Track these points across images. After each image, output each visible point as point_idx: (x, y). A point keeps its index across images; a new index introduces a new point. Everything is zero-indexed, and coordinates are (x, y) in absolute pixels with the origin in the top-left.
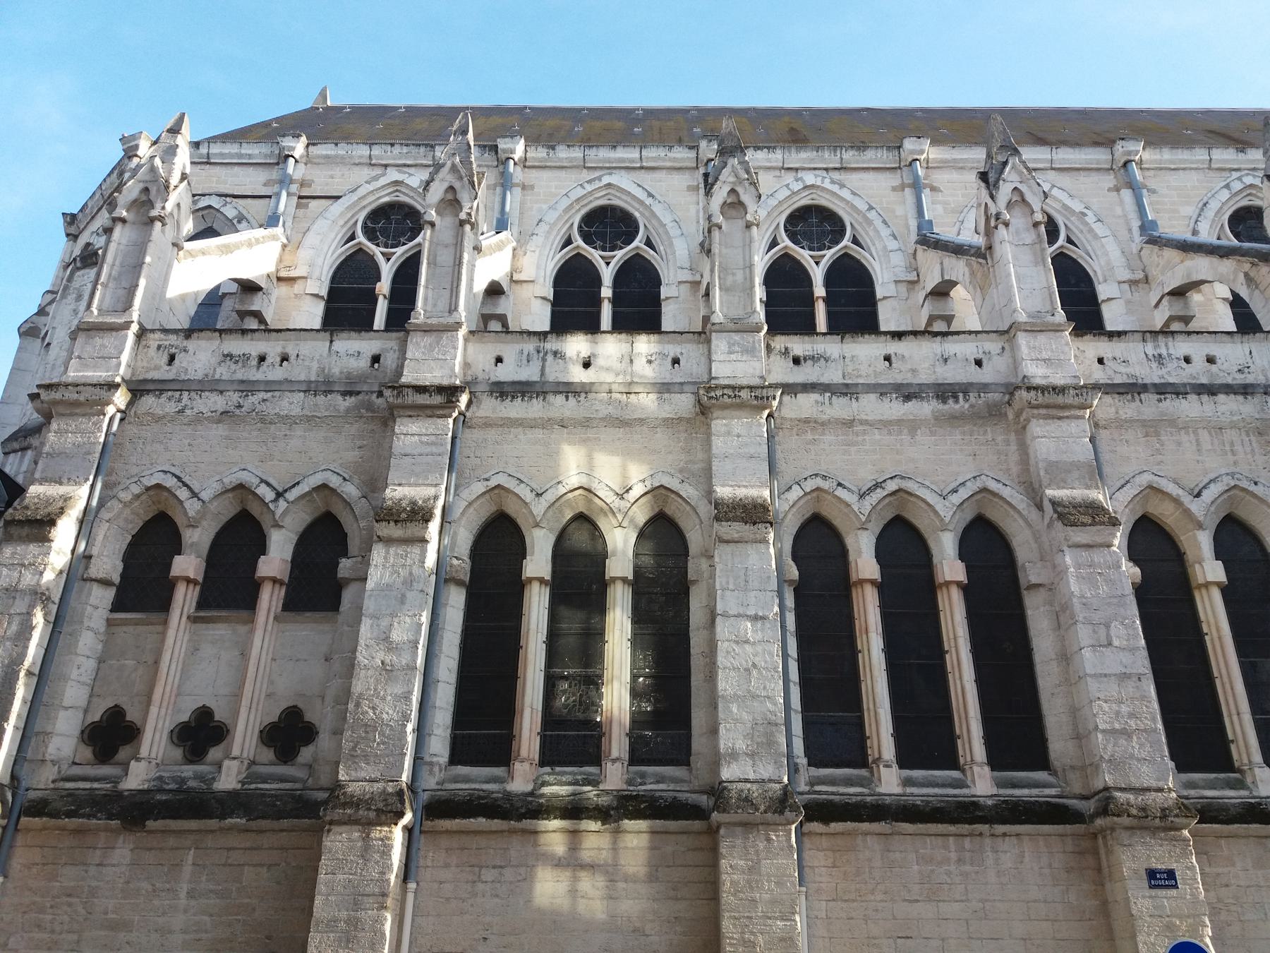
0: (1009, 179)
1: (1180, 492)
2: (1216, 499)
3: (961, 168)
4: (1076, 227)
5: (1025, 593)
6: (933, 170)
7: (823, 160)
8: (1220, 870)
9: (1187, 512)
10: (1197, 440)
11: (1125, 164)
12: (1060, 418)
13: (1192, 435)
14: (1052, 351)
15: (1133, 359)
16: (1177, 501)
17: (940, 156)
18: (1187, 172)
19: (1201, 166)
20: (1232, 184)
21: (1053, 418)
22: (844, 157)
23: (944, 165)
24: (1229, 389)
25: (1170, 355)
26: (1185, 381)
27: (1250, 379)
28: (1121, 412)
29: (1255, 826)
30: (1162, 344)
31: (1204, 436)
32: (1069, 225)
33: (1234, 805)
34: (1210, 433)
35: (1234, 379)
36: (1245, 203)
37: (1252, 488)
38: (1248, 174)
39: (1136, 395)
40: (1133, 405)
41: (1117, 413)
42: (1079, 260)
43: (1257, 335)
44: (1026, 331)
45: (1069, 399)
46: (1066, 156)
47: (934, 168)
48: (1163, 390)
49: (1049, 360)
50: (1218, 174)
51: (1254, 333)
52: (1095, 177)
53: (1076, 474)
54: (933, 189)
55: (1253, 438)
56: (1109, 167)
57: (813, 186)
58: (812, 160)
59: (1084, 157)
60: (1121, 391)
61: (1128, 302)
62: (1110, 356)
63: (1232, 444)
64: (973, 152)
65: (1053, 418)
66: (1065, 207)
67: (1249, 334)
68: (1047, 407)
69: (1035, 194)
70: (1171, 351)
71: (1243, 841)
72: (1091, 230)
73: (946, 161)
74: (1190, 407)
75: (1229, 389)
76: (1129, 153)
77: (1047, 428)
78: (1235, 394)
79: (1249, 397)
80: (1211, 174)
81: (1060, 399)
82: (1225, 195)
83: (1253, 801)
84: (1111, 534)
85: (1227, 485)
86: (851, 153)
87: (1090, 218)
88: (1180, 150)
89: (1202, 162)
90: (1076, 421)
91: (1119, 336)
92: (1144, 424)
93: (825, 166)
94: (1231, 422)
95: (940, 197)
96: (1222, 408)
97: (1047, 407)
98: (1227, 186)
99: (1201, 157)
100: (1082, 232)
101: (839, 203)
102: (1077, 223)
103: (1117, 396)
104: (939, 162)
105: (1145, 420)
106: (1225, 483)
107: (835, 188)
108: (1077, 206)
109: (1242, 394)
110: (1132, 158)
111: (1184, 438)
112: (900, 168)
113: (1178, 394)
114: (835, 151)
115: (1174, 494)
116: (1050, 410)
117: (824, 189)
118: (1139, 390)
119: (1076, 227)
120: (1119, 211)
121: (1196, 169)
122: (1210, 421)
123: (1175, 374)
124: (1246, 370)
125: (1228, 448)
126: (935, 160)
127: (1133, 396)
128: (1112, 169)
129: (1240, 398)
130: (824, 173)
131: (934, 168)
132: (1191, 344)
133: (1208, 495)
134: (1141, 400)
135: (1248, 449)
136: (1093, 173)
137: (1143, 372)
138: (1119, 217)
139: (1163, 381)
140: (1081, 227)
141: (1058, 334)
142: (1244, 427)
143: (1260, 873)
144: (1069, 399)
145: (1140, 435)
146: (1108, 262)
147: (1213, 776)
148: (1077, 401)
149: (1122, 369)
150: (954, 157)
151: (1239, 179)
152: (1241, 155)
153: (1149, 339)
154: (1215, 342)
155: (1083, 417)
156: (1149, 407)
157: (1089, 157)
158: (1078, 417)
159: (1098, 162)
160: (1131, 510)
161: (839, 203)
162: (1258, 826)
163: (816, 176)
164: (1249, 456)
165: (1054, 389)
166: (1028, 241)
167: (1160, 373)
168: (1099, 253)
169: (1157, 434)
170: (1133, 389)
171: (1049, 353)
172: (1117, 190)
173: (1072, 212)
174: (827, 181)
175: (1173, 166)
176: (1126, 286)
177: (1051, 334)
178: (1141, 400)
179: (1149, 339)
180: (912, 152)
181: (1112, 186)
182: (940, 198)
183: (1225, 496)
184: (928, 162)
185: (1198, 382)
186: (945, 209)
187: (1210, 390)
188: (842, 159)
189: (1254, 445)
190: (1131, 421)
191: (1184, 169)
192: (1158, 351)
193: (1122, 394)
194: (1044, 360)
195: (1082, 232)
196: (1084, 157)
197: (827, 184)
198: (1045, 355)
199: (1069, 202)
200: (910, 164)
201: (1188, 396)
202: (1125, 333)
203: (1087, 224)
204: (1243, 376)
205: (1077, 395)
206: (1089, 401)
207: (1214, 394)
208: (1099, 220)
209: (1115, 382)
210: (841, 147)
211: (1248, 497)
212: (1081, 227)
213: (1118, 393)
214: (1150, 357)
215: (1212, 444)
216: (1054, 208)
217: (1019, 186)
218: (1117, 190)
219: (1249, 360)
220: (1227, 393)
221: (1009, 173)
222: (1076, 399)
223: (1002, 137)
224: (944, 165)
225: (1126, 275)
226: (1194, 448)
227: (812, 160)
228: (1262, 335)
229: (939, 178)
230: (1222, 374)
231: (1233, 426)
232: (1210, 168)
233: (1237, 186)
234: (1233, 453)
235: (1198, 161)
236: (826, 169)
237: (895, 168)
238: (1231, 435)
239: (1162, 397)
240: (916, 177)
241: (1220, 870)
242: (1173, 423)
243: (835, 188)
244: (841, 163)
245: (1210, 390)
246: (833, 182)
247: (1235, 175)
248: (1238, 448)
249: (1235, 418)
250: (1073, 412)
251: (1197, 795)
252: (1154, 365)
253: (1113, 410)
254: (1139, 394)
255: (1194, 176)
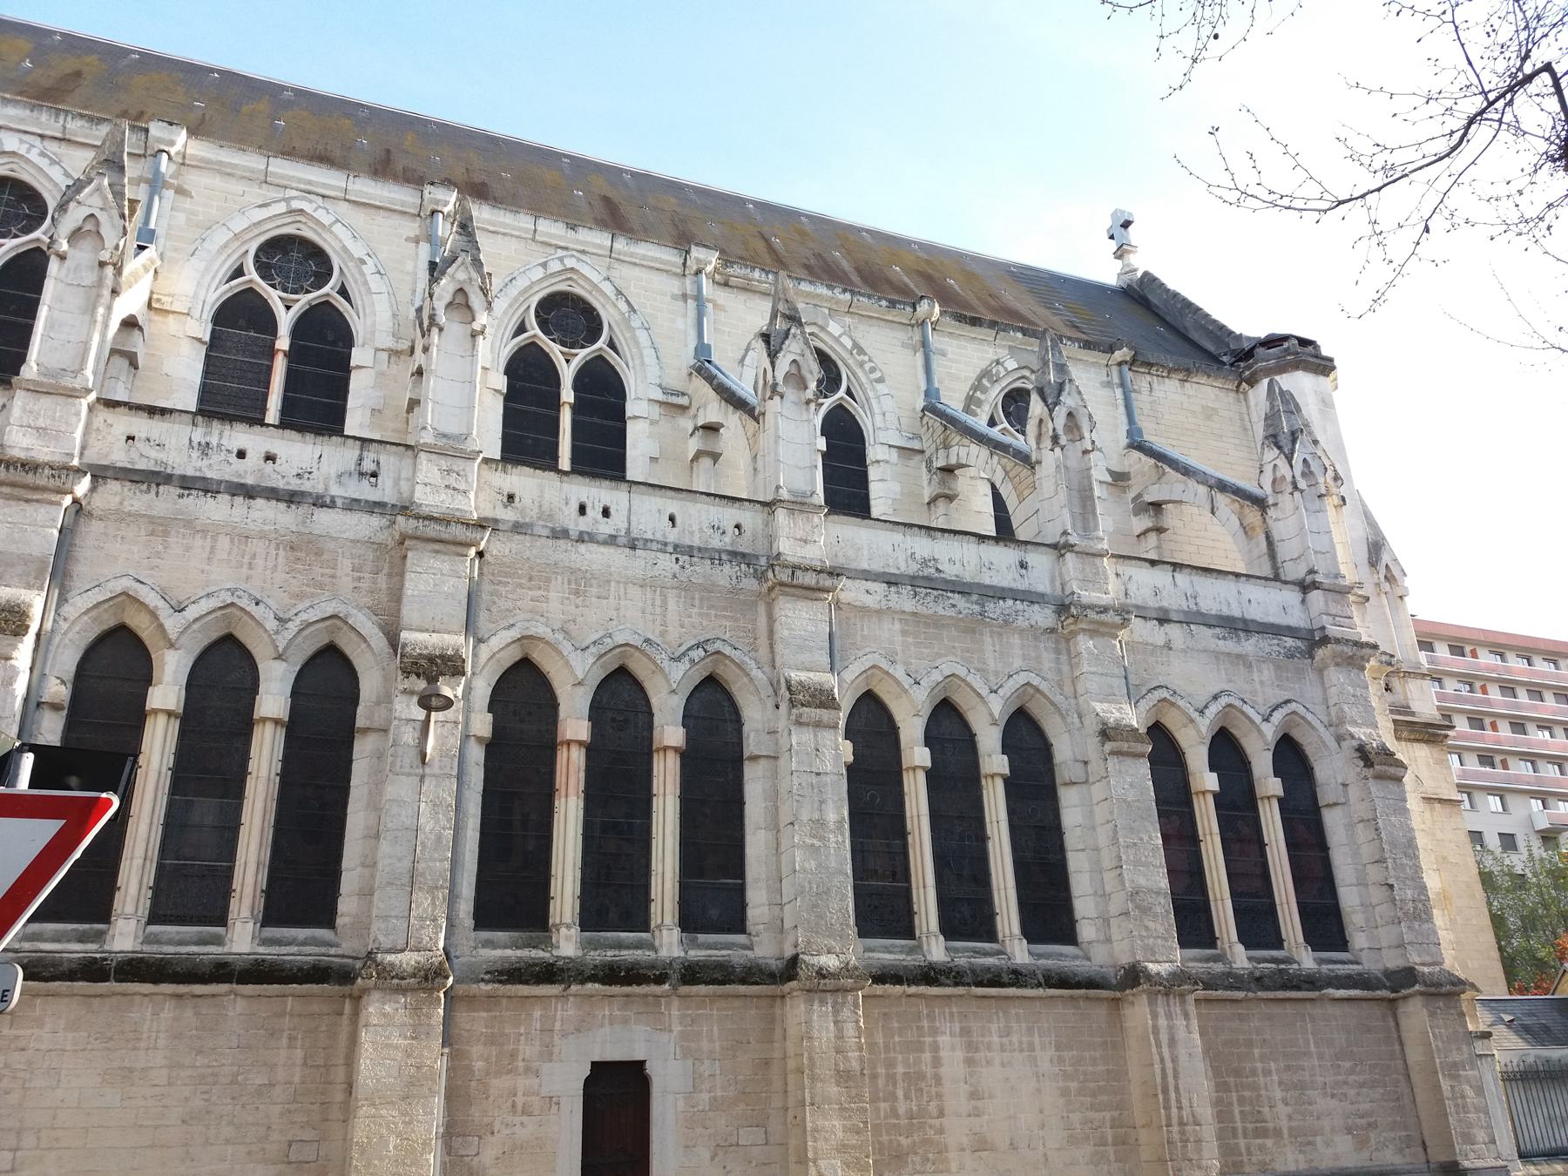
0: (88, 203)
1: (161, 604)
2: (202, 617)
3: (229, 174)
4: (353, 276)
5: (66, 705)
6: (191, 169)
7: (39, 124)
8: (22, 1032)
9: (161, 626)
10: (212, 548)
11: (433, 212)
12: (27, 501)
13: (209, 540)
14: (53, 419)
15: (171, 442)
16: (153, 614)
17: (202, 154)
18: (506, 238)
19: (524, 236)
20: (551, 264)
21: (19, 499)
22: (68, 126)
23: (204, 166)
24: (273, 494)
25: (219, 445)
26: (227, 478)
27: (306, 486)
28: (126, 503)
29: (81, 983)
30: (216, 432)
31: (224, 543)
32: (345, 270)
33: (70, 961)
34: (232, 541)
35: (288, 483)
36: (563, 287)
37: (252, 608)
38: (573, 256)
39: (154, 486)
40: (146, 497)
41: (121, 503)
42: (345, 314)
43: (334, 438)
44: (28, 390)
45: (42, 479)
46: (365, 189)
47: (193, 166)
48: (188, 484)
49: (45, 429)
50: (540, 248)
51: (330, 436)
52: (396, 220)
53: (19, 569)
54: (180, 191)
55: (281, 552)
56: (416, 212)
57: (13, 154)
58: (22, 120)
59: (386, 194)
60: (136, 478)
61: (381, 374)
62: (144, 436)
63: (254, 556)
64: (247, 158)
65: (19, 499)
66: (345, 248)
67: (323, 435)
68: (13, 485)
69: (113, 226)
70: (224, 442)
71: (66, 1000)
72: (366, 283)
73: (208, 161)
74: (216, 509)
75: (273, 494)
76: (437, 202)
77: (6, 510)
78: (278, 500)
79: (293, 507)
80: (534, 247)
81: (30, 478)
82: (539, 273)
83: (98, 956)
84: (11, 645)
85: (224, 601)
86: (79, 123)
87: (369, 268)
88: (502, 212)
89: (526, 230)
90: (48, 506)
91: (163, 415)
92: (151, 520)
93: (39, 132)
94: (261, 531)
95: (187, 203)
96: (254, 514)
97: (13, 485)
98: (544, 265)
99: (526, 225)
100: (356, 282)
101: (47, 184)
102: (355, 271)
103: (129, 484)
104: (200, 161)
105: (153, 517)
106: (221, 599)
107: (43, 163)
108: (358, 251)
109: (286, 501)
110: (440, 208)
111: (198, 541)
112: (144, 156)
113: (206, 491)
114: (57, 116)
115: (152, 605)
116: (17, 489)
117: (28, 161)
118: (159, 481)
119: (353, 276)
120: (409, 266)
121: (518, 237)
122: (235, 528)
123: (217, 468)
124: (306, 476)
125: (246, 560)
126: (194, 157)
127: (149, 486)
128: (419, 215)
129: (282, 506)
130: (37, 141)
131: (193, 166)
132: (252, 436)
133: (192, 612)
134: (157, 493)
135: (270, 564)
136: (395, 217)
137: (177, 461)
138: (407, 273)
139: (198, 474)
140: (357, 276)
141: (70, 400)
142: (276, 539)
143: (70, 1035)
144: (42, 479)
145: (143, 533)
146: (374, 324)
147: (87, 926)
148: (52, 483)
149: (154, 454)
150: (220, 158)
151: (561, 259)
152: (571, 233)
153: (200, 423)
154: (283, 439)
155: (59, 504)
156: (166, 501)
157: (393, 195)
158: (52, 503)
159: (403, 203)
160: (95, 619)
161: (47, 184)
162: (85, 984)
163: (22, 141)
164: (268, 572)
165: (23, 465)
166: (87, 282)
167: (199, 464)
168: (367, 311)
169: (166, 533)
170: (155, 478)
171: (48, 422)
172: (417, 241)
173: (351, 256)
174: (35, 151)
175: (491, 228)
176: (385, 355)
177: (61, 399)
178: (157, 493)
179: (200, 423)
180: (160, 140)
181: (412, 235)
182: (187, 206)
183: (219, 613)
184: (184, 157)
185: (242, 481)
186: (188, 219)
187: (248, 492)
188: (65, 128)
189: (280, 560)
190: (137, 516)
191: (504, 234)
192: (208, 439)
193: (137, 482)
194: (38, 429)
195: (356, 282)
196: (386, 194)
197: (33, 156)
198: (41, 423)
199: (349, 244)
200: (154, 156)
201: (219, 496)
202: (171, 411)
203: (363, 274)
204: (299, 481)
205: (53, 476)
206: (68, 485)
207: (252, 497)
208: (379, 272)
209: (137, 467)
210: (67, 112)
211: (246, 618)
212: (357, 276)
213: (132, 481)
214: (195, 444)
215: (229, 554)
216: (332, 247)
217: (98, 213)
218: (417, 241)
219: (315, 465)
220: (268, 499)
221: (91, 195)
222: (52, 480)
223: (114, 149)
224: (204, 166)
225: (388, 342)
226: (205, 555)
227: (22, 120)
228: (339, 439)
229: (193, 180)
230: (275, 476)
231: (263, 536)
232: (533, 240)
233: (555, 266)
234: (250, 566)
235: (520, 229)
236: (42, 136)
237: (140, 155)
238: (258, 546)
239: (187, 492)
240: (157, 172)
241: (22, 1032)
242: (189, 524)
243: (43, 163)
244: (64, 132)
245: (248, 492)
246: (43, 154)
247: (560, 253)
248: (259, 562)
249: (266, 528)
250: (46, 496)
251: (31, 948)
252: (195, 454)
253: (117, 499)
254: (158, 485)
255: (513, 245)
